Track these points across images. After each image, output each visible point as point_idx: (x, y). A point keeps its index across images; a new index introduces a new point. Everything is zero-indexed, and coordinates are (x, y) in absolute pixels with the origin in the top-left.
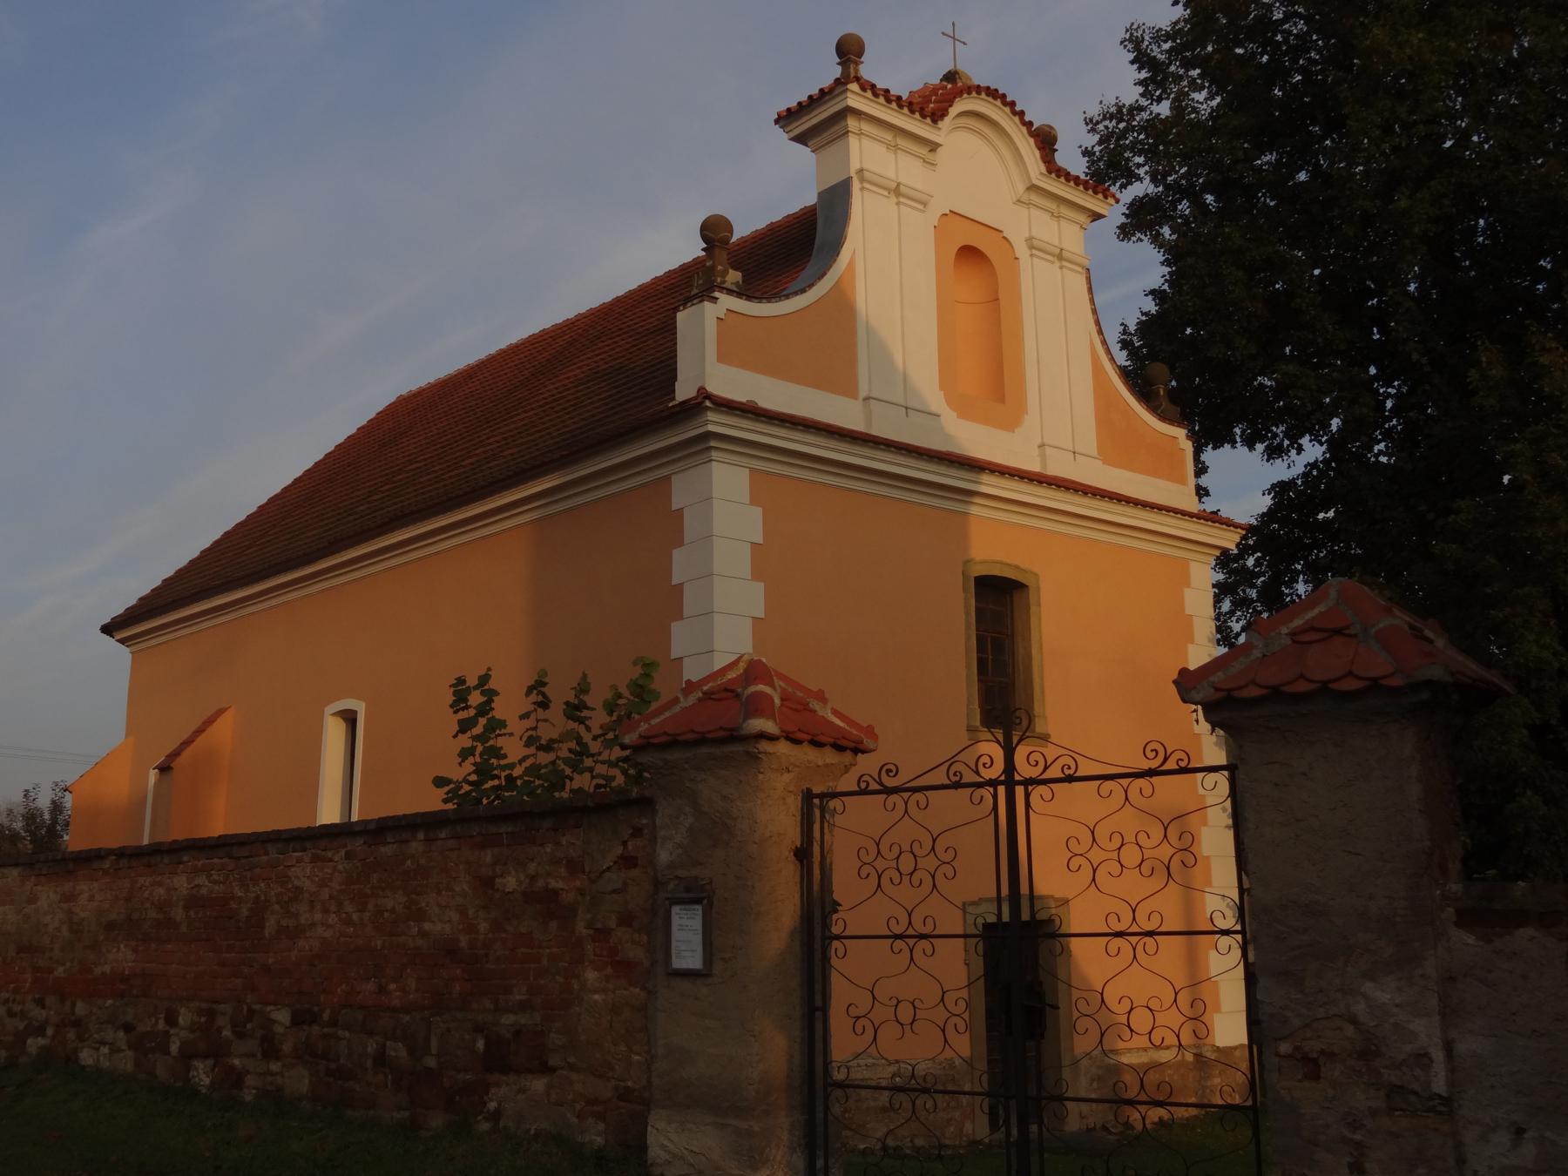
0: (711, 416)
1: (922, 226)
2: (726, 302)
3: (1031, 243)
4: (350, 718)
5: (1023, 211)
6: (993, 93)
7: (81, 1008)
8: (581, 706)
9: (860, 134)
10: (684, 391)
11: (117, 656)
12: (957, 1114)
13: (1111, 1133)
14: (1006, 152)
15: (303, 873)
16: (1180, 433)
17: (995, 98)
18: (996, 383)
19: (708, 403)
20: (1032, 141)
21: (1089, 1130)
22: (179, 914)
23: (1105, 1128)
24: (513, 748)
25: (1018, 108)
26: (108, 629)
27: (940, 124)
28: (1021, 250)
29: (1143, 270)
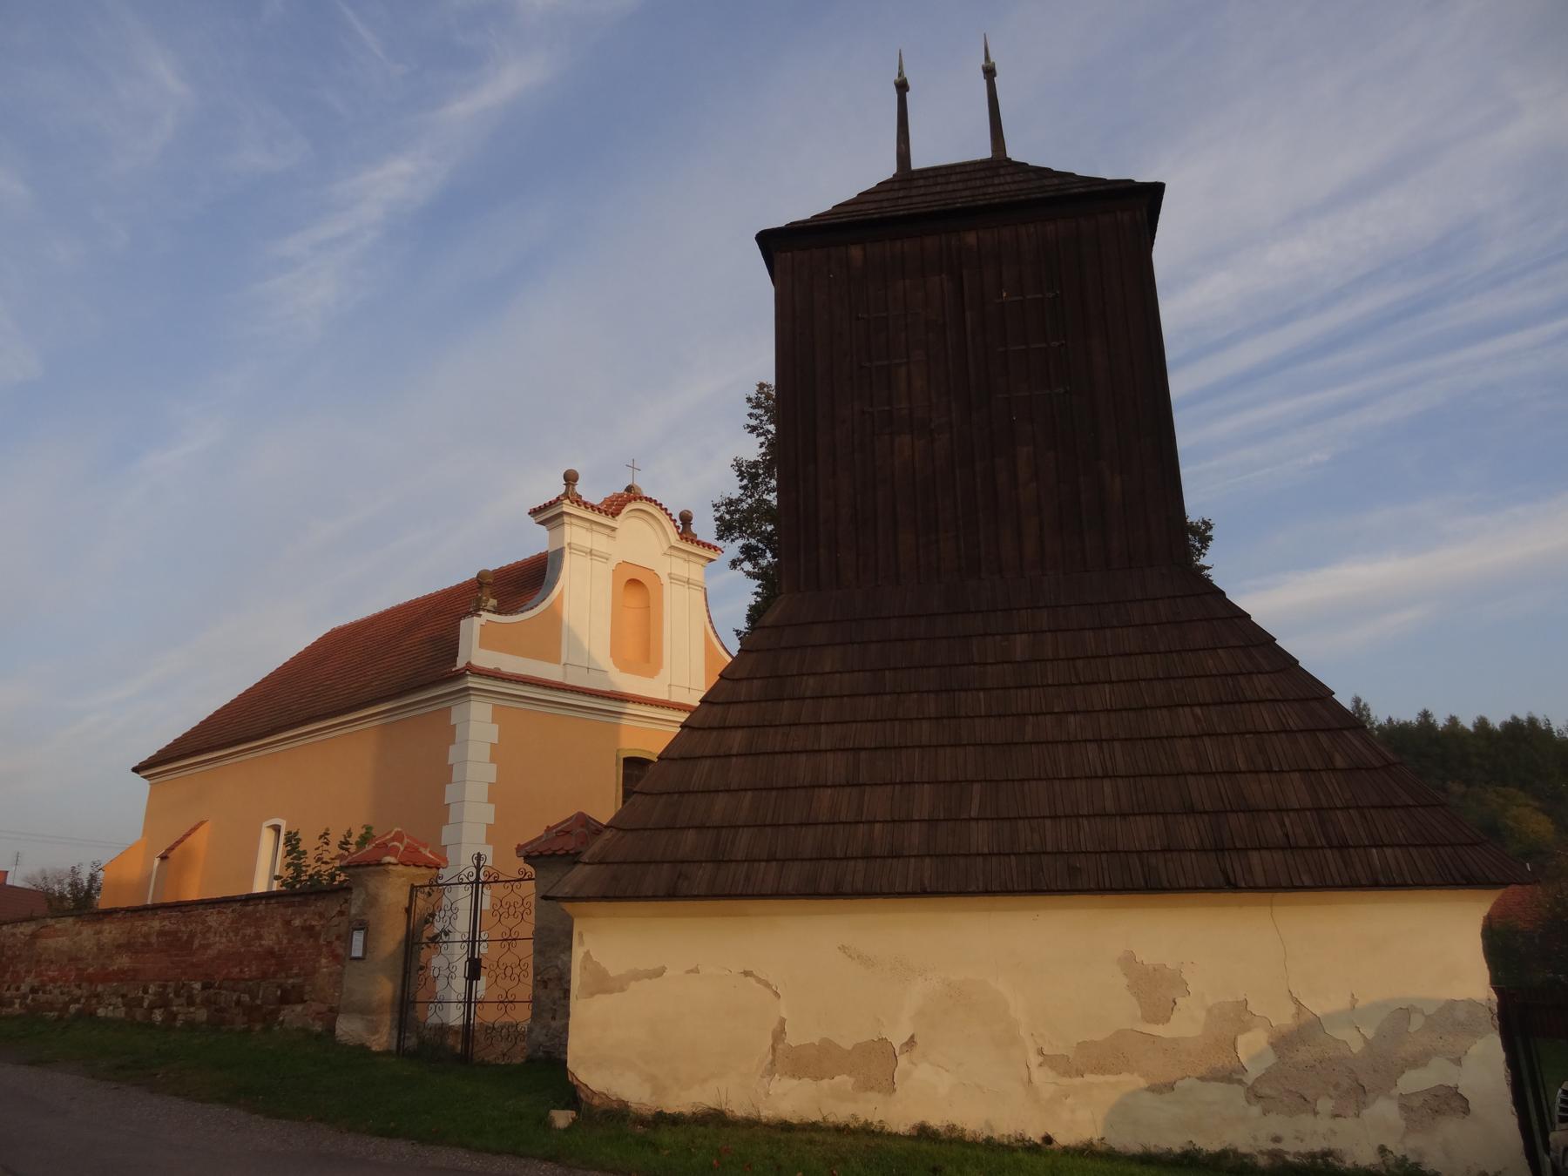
1: (604, 571)
2: (486, 616)
3: (670, 576)
4: (277, 829)
5: (668, 559)
6: (650, 500)
7: (100, 988)
8: (347, 843)
10: (461, 663)
11: (142, 785)
15: (213, 919)
22: (153, 939)
24: (310, 860)
26: (135, 770)
28: (665, 580)
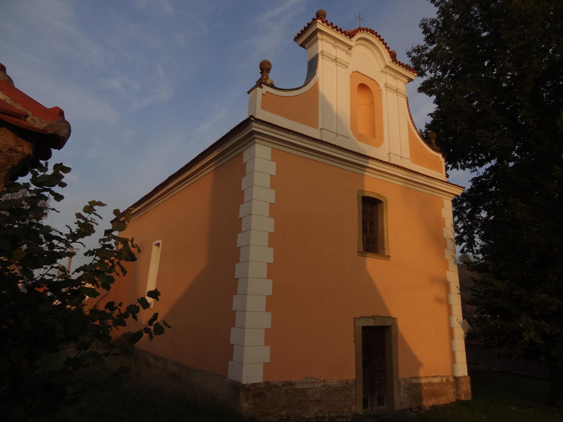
0: (254, 124)
3: (386, 86)
5: (383, 75)
9: (322, 39)
12: (349, 403)
13: (413, 412)
14: (378, 55)
16: (440, 155)
17: (373, 34)
18: (374, 133)
19: (252, 119)
20: (389, 54)
21: (404, 410)
23: (410, 409)
25: (381, 38)
27: (352, 39)
28: (382, 87)
29: (428, 106)
